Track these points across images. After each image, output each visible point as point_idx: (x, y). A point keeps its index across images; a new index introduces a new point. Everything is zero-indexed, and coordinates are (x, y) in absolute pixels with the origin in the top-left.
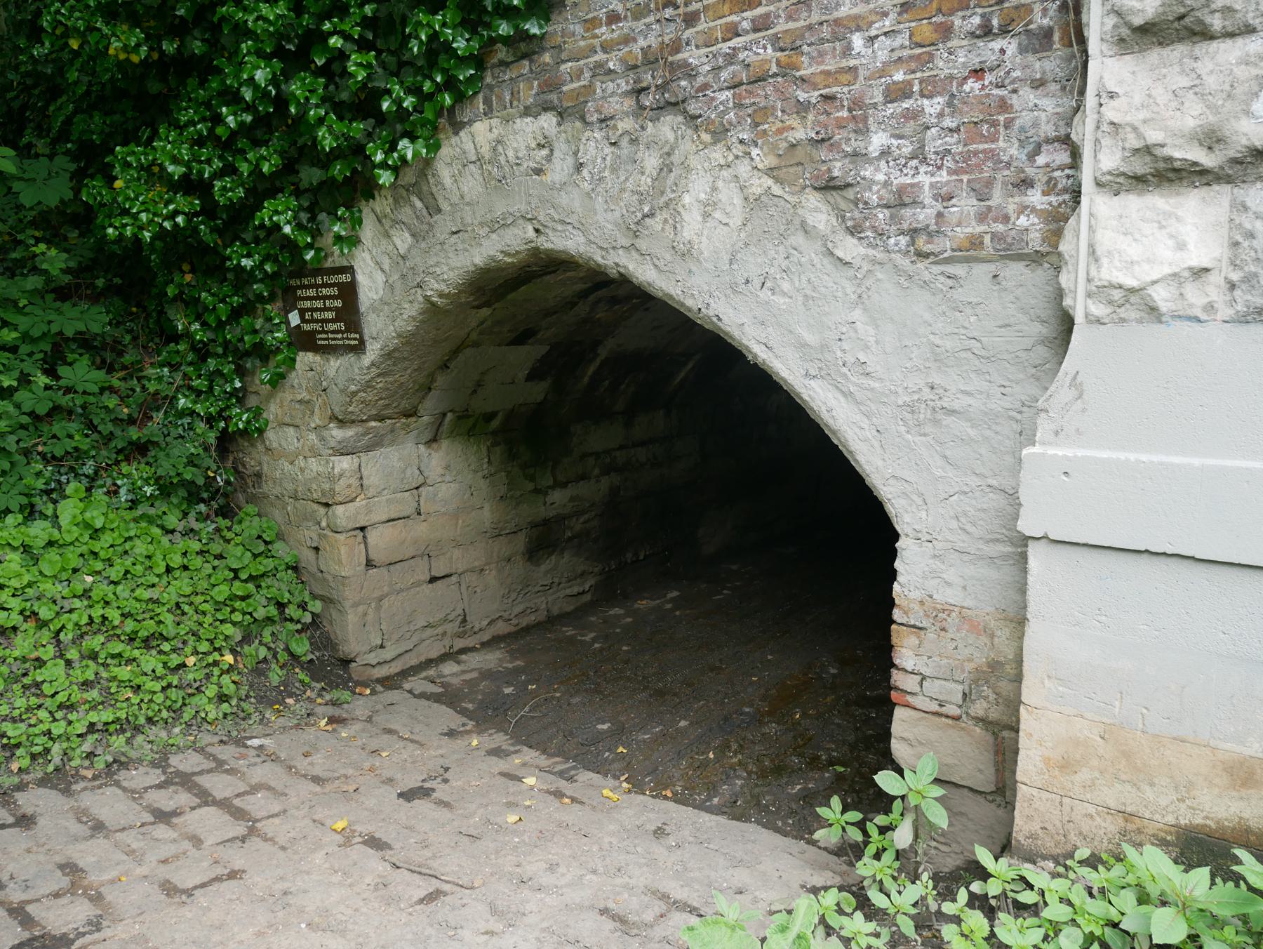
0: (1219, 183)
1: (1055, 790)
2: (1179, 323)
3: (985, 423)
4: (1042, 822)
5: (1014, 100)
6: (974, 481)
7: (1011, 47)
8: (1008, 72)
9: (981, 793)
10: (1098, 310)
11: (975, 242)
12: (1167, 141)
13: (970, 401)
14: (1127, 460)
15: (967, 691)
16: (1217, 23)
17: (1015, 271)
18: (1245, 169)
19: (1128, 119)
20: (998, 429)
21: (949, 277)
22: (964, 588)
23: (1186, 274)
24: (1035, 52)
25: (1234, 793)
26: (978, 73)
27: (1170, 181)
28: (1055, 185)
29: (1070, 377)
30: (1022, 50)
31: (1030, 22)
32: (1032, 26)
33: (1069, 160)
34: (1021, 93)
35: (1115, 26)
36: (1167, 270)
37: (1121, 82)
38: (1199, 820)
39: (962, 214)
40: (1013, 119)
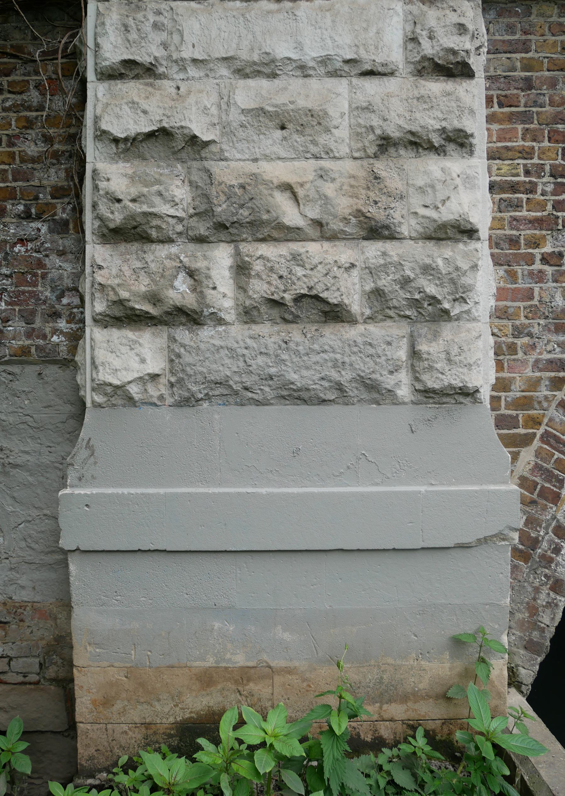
0: (161, 325)
1: (102, 721)
2: (145, 407)
3: (39, 472)
4: (96, 746)
5: (47, 261)
6: (35, 513)
7: (44, 228)
8: (42, 244)
9: (59, 733)
10: (99, 399)
11: (25, 351)
12: (131, 298)
13: (28, 457)
14: (123, 494)
15: (42, 662)
16: (154, 234)
17: (52, 371)
18: (174, 318)
19: (109, 282)
20: (48, 475)
21: (9, 374)
22: (34, 588)
23: (147, 378)
24: (59, 233)
25: (204, 693)
26: (22, 241)
27: (135, 321)
28: (74, 317)
29: (85, 442)
30: (51, 231)
31: (55, 214)
32: (56, 217)
33: (80, 303)
34: (51, 257)
35: (99, 226)
36: (136, 375)
37: (104, 260)
38: (187, 716)
39: (15, 332)
40: (47, 273)
